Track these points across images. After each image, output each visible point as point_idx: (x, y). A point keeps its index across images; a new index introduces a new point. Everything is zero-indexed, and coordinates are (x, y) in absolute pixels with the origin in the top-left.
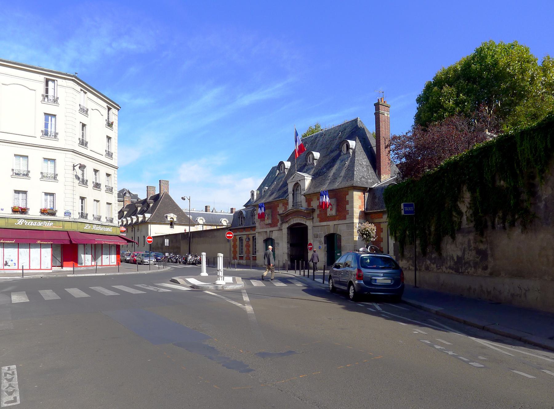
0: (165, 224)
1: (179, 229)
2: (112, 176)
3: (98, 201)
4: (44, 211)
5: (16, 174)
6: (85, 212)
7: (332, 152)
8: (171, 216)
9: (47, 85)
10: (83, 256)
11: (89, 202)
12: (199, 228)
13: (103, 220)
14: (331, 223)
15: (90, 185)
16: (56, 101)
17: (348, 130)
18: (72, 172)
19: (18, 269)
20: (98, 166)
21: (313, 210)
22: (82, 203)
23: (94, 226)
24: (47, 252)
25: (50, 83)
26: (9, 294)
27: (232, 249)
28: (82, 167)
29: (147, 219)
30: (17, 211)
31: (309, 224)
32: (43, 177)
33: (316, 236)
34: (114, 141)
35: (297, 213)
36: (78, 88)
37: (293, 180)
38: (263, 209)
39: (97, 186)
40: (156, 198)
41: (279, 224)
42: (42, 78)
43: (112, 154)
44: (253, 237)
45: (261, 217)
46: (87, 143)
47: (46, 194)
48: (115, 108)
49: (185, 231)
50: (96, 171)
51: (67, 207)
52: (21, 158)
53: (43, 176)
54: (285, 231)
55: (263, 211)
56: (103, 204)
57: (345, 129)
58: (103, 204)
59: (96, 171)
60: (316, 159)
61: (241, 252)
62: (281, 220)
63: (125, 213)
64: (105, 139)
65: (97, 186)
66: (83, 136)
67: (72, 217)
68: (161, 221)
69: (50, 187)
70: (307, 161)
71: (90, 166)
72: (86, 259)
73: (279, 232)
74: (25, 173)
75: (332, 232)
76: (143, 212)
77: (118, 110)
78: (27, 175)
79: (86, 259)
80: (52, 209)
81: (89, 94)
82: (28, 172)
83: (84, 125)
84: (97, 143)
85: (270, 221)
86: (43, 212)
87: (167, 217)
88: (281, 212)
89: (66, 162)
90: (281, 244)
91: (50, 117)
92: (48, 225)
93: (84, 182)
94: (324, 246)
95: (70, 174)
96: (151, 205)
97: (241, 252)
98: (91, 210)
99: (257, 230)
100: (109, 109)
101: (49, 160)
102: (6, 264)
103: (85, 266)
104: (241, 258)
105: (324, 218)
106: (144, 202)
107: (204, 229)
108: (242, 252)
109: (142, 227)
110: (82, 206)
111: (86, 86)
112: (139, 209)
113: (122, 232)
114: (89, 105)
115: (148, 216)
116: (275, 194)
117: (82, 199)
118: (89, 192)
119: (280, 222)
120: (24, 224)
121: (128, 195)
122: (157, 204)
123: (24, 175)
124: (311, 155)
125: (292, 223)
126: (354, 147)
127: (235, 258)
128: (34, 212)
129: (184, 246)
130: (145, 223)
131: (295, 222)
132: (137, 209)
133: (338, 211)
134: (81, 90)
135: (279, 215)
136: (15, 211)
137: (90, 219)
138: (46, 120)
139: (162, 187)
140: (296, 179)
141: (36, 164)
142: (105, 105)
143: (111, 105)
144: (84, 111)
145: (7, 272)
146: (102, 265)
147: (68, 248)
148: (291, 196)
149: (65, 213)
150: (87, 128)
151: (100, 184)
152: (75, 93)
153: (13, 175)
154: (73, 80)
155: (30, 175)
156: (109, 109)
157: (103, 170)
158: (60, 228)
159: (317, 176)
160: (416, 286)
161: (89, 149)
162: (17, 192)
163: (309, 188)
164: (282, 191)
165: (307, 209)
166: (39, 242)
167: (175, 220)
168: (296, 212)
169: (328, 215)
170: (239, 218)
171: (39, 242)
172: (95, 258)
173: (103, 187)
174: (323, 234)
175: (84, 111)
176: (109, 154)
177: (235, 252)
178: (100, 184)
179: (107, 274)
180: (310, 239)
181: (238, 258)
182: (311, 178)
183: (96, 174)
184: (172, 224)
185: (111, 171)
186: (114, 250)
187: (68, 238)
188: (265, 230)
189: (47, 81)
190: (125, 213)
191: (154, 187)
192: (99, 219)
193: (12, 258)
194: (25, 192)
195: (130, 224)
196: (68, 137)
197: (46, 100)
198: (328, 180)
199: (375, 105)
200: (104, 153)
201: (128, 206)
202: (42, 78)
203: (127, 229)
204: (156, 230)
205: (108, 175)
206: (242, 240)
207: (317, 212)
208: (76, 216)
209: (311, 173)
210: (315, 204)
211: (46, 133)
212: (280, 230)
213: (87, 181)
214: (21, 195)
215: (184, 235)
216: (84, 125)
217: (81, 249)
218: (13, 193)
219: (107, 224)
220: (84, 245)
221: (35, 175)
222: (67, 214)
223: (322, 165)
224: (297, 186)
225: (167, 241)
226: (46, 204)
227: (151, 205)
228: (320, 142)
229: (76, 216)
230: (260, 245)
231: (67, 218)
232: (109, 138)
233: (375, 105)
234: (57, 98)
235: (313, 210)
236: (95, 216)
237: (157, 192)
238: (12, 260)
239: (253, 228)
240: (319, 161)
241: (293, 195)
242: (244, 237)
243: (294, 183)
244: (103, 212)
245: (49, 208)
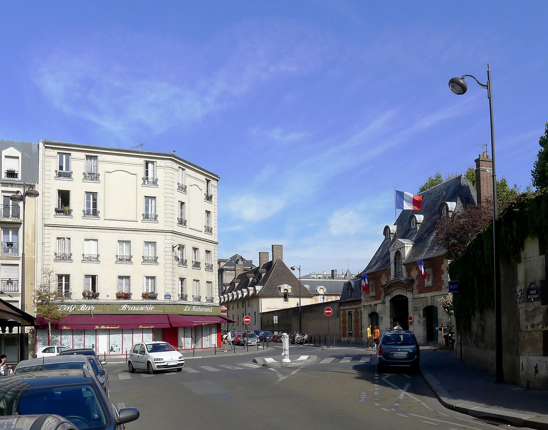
0: (278, 296)
1: (292, 303)
2: (212, 253)
3: (197, 281)
4: (146, 295)
5: (119, 260)
6: (184, 293)
7: (434, 214)
8: (286, 287)
9: (147, 167)
10: (182, 339)
11: (189, 283)
12: (319, 300)
13: (203, 300)
14: (429, 295)
15: (190, 264)
16: (155, 183)
17: (452, 189)
18: (170, 253)
19: (122, 355)
20: (196, 244)
21: (412, 281)
22: (182, 285)
23: (194, 308)
24: (151, 335)
25: (150, 165)
26: (116, 374)
27: (342, 325)
28: (181, 247)
29: (257, 292)
30: (121, 297)
31: (409, 296)
32: (145, 261)
33: (416, 309)
34: (213, 216)
35: (397, 284)
36: (176, 166)
38: (366, 280)
39: (197, 265)
40: (269, 266)
41: (382, 296)
42: (142, 161)
43: (212, 229)
44: (349, 312)
45: (366, 288)
46: (186, 221)
47: (147, 278)
48: (214, 179)
50: (195, 249)
51: (166, 289)
52: (124, 244)
53: (145, 260)
54: (388, 304)
55: (367, 282)
56: (203, 283)
57: (449, 188)
58: (203, 283)
59: (195, 249)
60: (419, 223)
63: (237, 284)
64: (205, 214)
65: (197, 265)
66: (182, 214)
67: (172, 299)
68: (273, 294)
69: (151, 270)
70: (410, 225)
71: (189, 244)
72: (186, 342)
74: (128, 258)
75: (429, 304)
76: (253, 285)
77: (218, 180)
78: (130, 260)
79: (186, 342)
80: (153, 293)
81: (187, 170)
82: (131, 257)
83: (182, 204)
84: (196, 220)
85: (373, 294)
86: (145, 296)
87: (280, 288)
88: (384, 283)
89: (164, 243)
91: (150, 200)
92: (150, 309)
93: (183, 263)
94: (423, 320)
95: (170, 256)
96: (263, 275)
97: (351, 329)
98: (190, 292)
100: (208, 181)
101: (150, 243)
102: (112, 350)
103: (185, 349)
104: (350, 334)
105: (423, 289)
106: (256, 271)
107: (325, 301)
109: (253, 302)
110: (182, 287)
111: (184, 163)
112: (251, 279)
113: (222, 311)
114: (188, 182)
115: (258, 288)
116: (379, 263)
117: (182, 280)
118: (189, 273)
120: (127, 309)
121: (240, 262)
122: (269, 273)
123: (127, 260)
124: (414, 219)
125: (394, 295)
126: (453, 210)
127: (344, 336)
128: (136, 297)
129: (295, 323)
130: (256, 297)
132: (249, 280)
133: (434, 281)
134: (180, 167)
135: (382, 286)
136: (119, 296)
137: (190, 300)
138: (147, 203)
139: (275, 253)
140: (397, 247)
141: (138, 250)
142: (203, 178)
143: (211, 177)
144: (183, 189)
145: (113, 357)
146: (202, 348)
147: (169, 331)
148: (392, 265)
149: (165, 296)
150: (186, 205)
151: (199, 263)
152: (173, 172)
153: (117, 261)
154: (170, 159)
155: (132, 260)
156: (208, 181)
157: (203, 247)
158: (161, 312)
159: (418, 244)
160: (461, 359)
161: (188, 228)
162: (121, 277)
163: (409, 257)
164: (386, 260)
165: (407, 280)
166: (141, 327)
167: (290, 291)
168: (397, 283)
169: (426, 286)
170: (348, 289)
171: (141, 327)
172: (195, 341)
173: (203, 266)
174: (421, 306)
175: (183, 189)
176: (209, 230)
177: (344, 328)
178: (199, 263)
179: (204, 357)
180: (411, 315)
181: (348, 335)
182: (412, 245)
183: (195, 253)
184: (286, 296)
185: (210, 247)
186: (214, 330)
187: (168, 322)
188: (370, 303)
189: (147, 163)
190: (237, 284)
191: (268, 253)
192: (199, 300)
193: (117, 343)
194: (128, 277)
195: (241, 298)
196: (167, 219)
197: (146, 183)
198: (427, 247)
199: (476, 161)
200: (204, 229)
201: (240, 276)
202: (142, 161)
203: (228, 308)
204: (268, 305)
205: (208, 252)
206: (351, 314)
207: (416, 283)
208: (175, 298)
209: (414, 239)
210: (414, 274)
211: (146, 217)
212: (384, 303)
213: (186, 261)
214: (124, 280)
215: (299, 311)
216: (182, 204)
217: (181, 333)
218: (118, 279)
219: (207, 304)
220: (184, 327)
221: (137, 259)
222: (167, 296)
223: (425, 230)
224: (398, 254)
225: (276, 319)
226: (148, 290)
227: (263, 275)
228: (425, 203)
229: (175, 298)
230: (365, 320)
231: (167, 301)
232: (208, 212)
233: (476, 161)
234: (157, 180)
235: (412, 281)
236: (195, 297)
237: (270, 259)
238: (117, 346)
239: (360, 301)
240: (423, 225)
241: (395, 264)
242: (353, 311)
243: (396, 251)
244: (203, 291)
245: (150, 291)
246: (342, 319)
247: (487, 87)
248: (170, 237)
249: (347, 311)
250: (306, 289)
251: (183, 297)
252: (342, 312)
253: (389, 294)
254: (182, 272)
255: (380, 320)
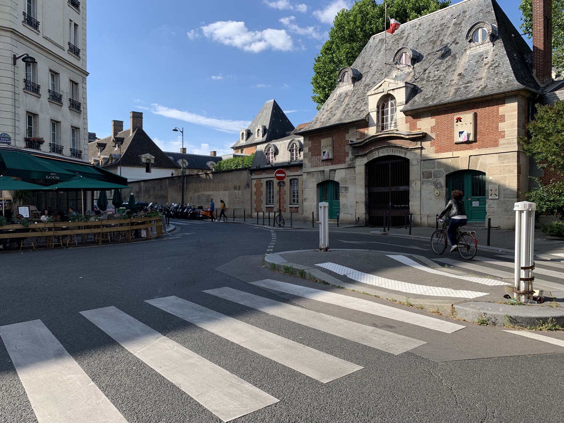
37: (380, 90)
39: (55, 98)
41: (348, 159)
49: (172, 174)
59: (54, 74)
61: (269, 201)
62: (353, 154)
66: (29, 7)
73: (348, 171)
90: (351, 189)
93: (32, 88)
98: (44, 131)
99: (304, 170)
108: (270, 201)
119: (350, 156)
131: (381, 155)
161: (41, 35)
181: (264, 210)
188: (321, 169)
200: (67, 48)
212: (352, 167)
225: (8, 241)
243: (380, 95)
246: (254, 190)
247: (182, 132)
248: (9, 40)
249: (264, 182)
250: (170, 160)
251: (33, 142)
252: (254, 182)
253: (365, 155)
254: (30, 102)
255: (342, 191)
